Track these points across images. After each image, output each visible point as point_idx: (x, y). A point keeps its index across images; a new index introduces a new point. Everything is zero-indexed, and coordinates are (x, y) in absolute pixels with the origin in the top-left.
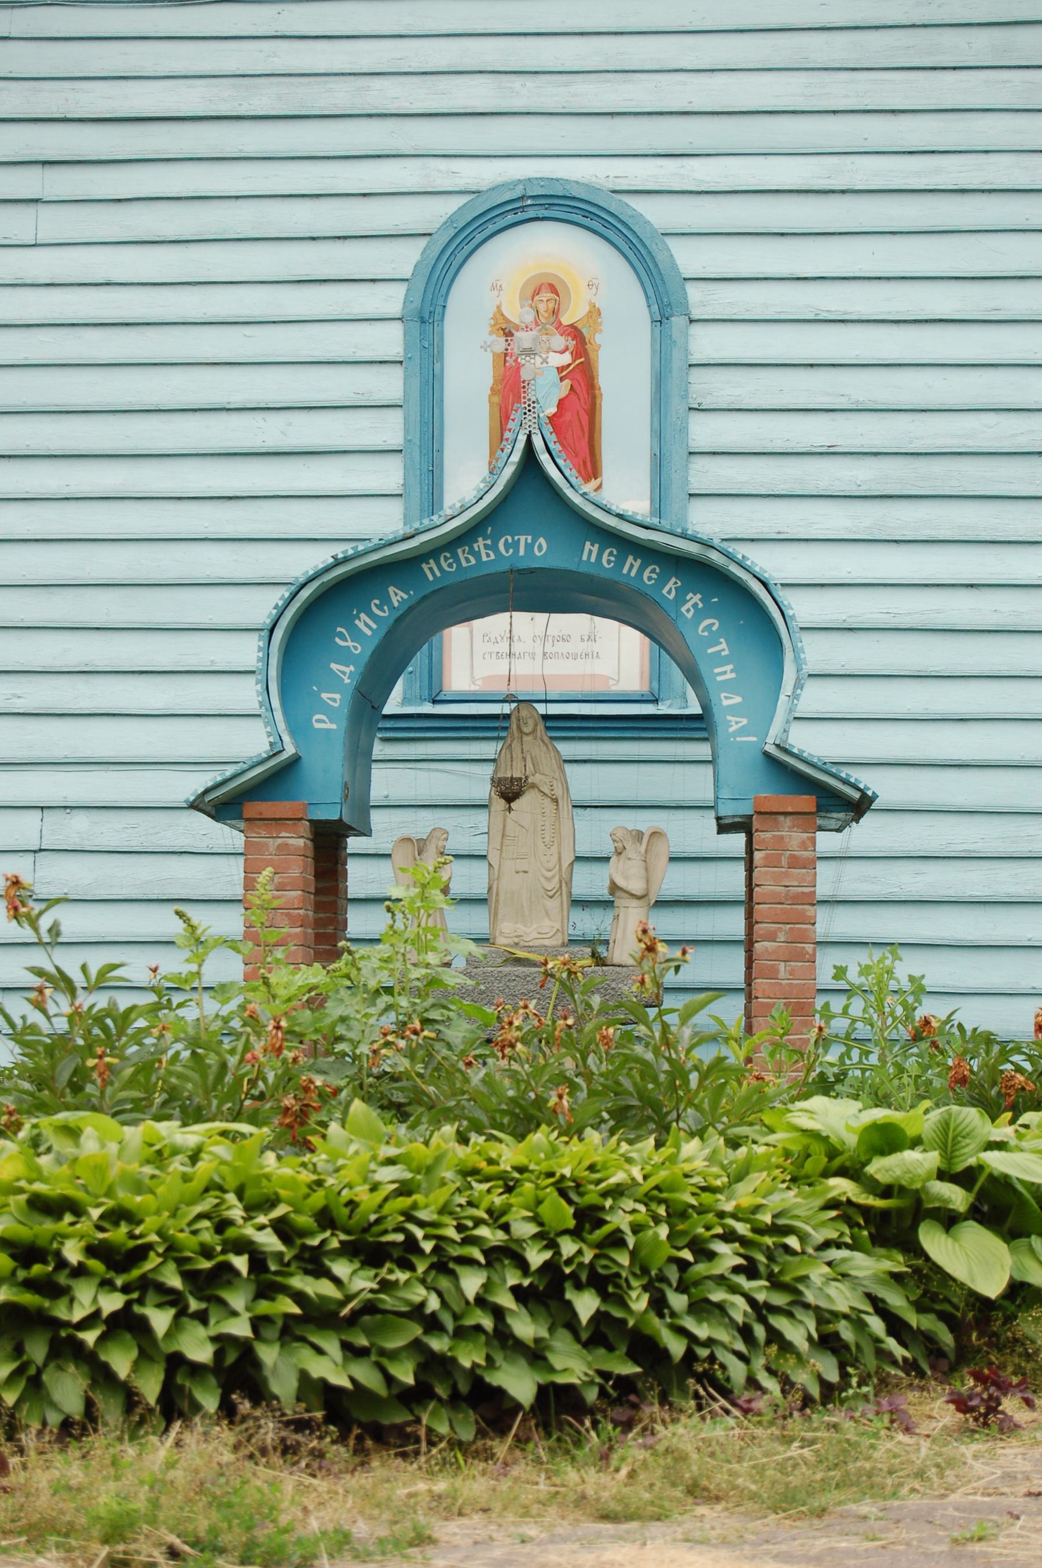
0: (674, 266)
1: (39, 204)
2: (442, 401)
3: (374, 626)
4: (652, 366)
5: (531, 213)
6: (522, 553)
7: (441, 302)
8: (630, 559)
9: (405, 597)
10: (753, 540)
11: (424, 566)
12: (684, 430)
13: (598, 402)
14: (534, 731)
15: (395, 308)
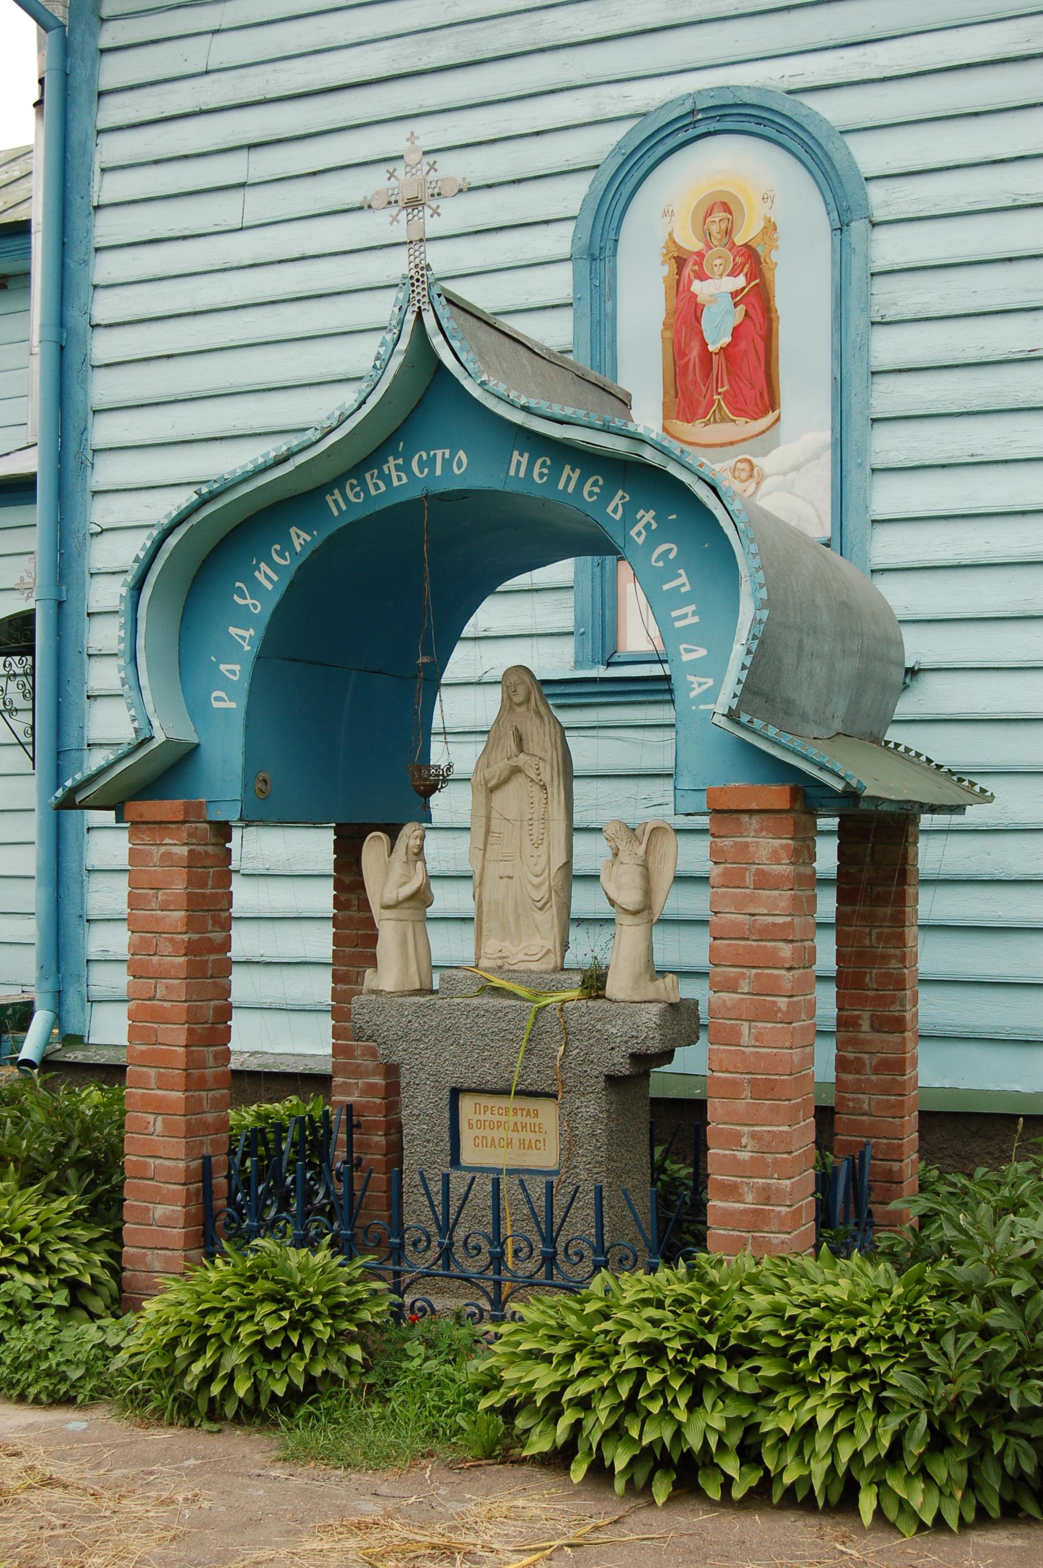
0: (853, 165)
1: (247, 188)
2: (614, 341)
3: (275, 578)
4: (833, 279)
5: (702, 129)
6: (438, 472)
7: (612, 236)
8: (567, 469)
9: (308, 538)
10: (944, 466)
11: (329, 499)
12: (865, 347)
13: (774, 326)
14: (528, 700)
15: (565, 249)
